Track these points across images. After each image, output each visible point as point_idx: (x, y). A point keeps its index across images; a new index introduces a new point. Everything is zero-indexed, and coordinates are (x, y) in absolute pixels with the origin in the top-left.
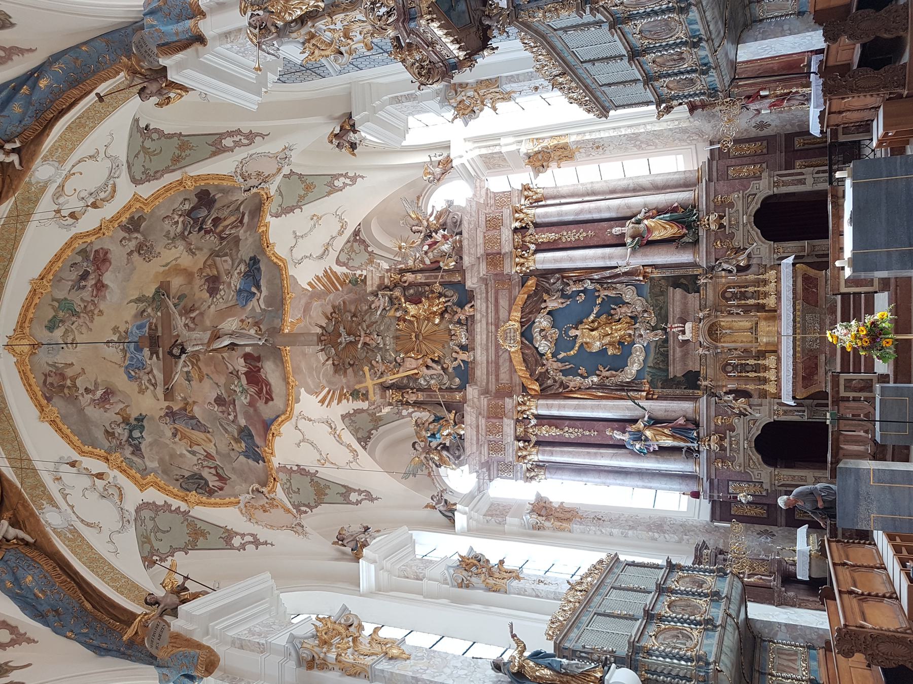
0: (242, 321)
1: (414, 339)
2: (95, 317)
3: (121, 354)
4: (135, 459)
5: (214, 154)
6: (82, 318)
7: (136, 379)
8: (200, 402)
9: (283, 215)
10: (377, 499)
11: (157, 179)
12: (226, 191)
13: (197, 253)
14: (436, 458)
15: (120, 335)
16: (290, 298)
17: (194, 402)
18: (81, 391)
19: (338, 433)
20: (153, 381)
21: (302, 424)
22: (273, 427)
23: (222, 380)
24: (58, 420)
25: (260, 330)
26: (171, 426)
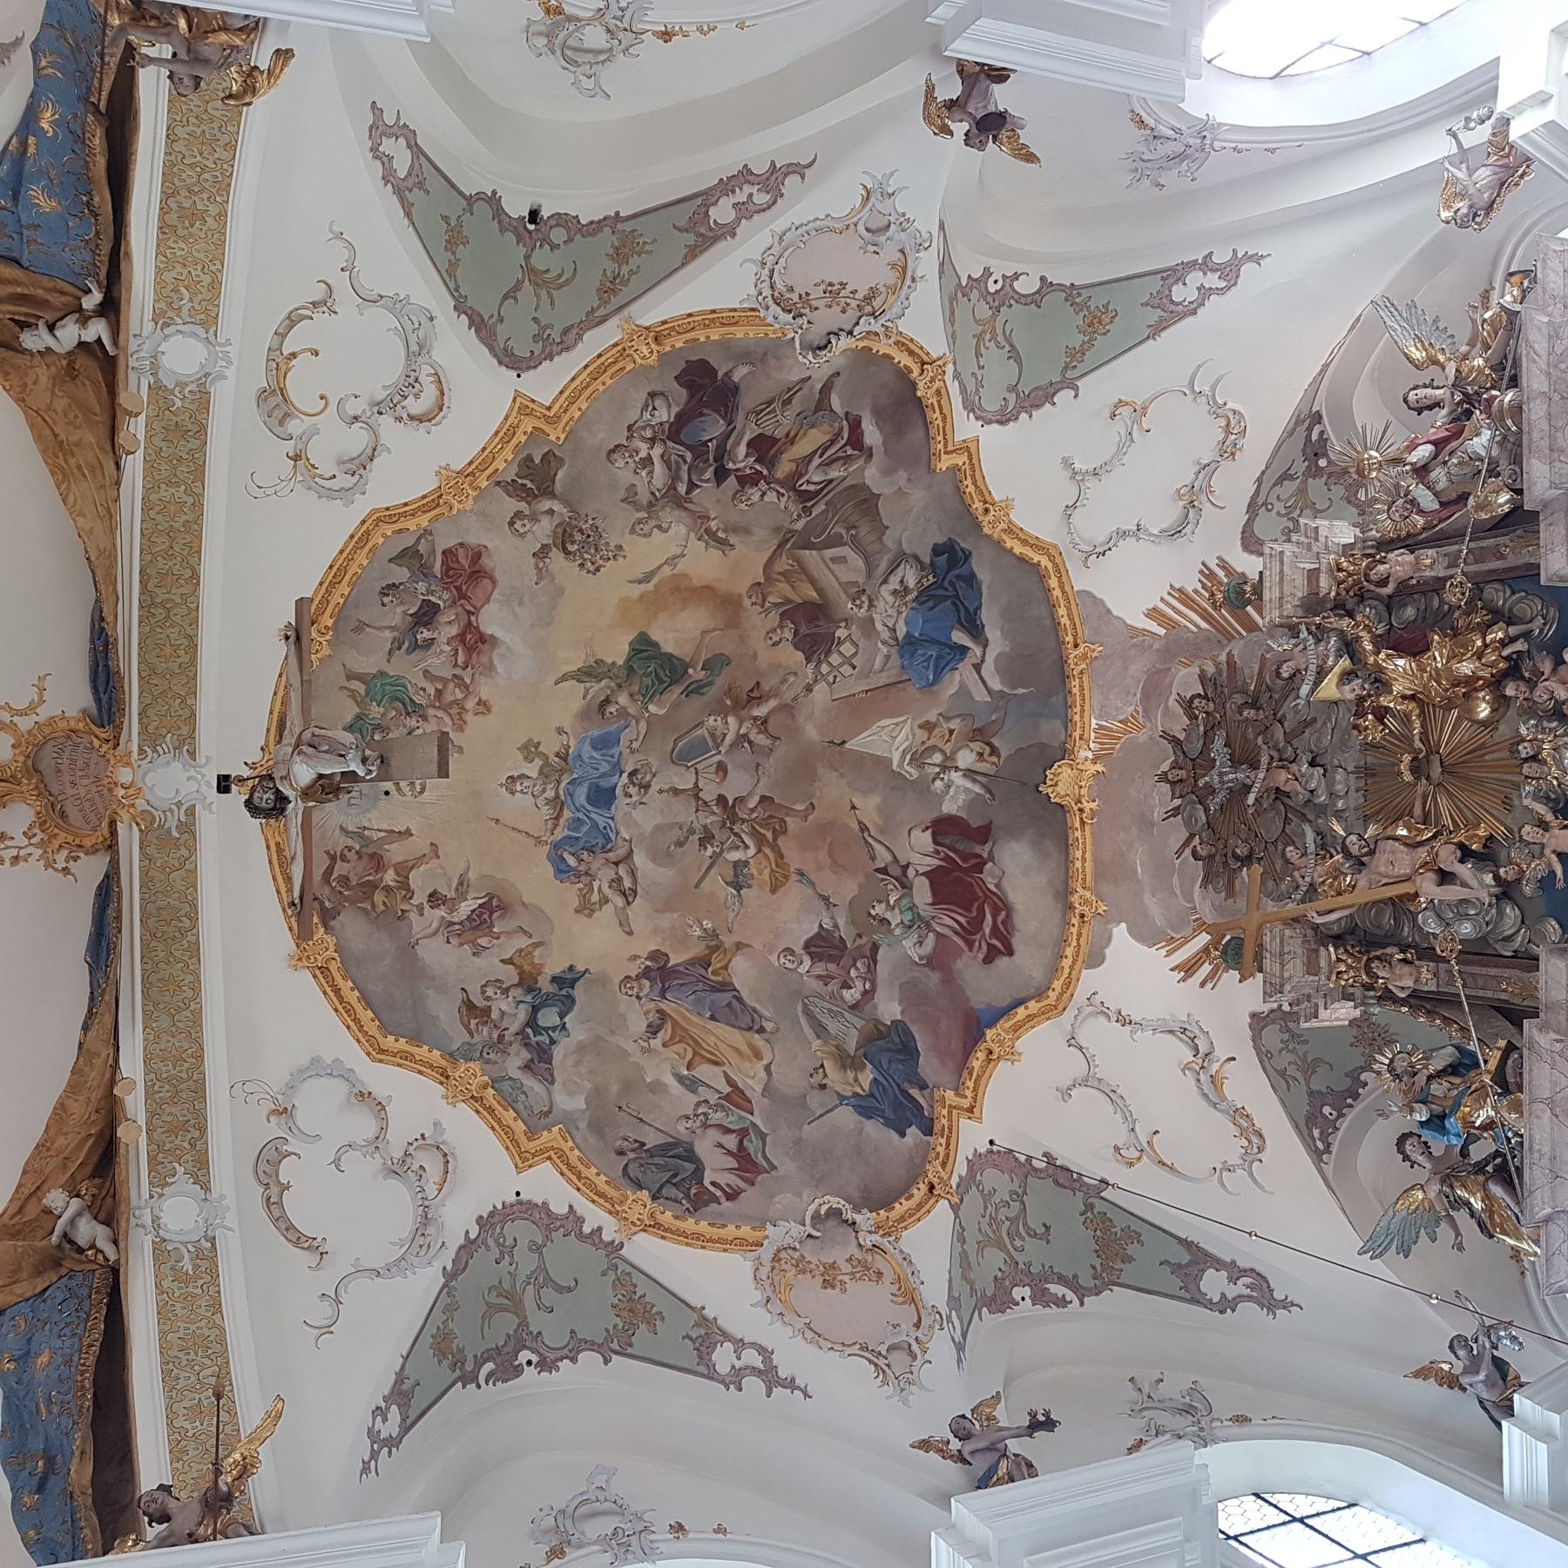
0: (928, 727)
1: (1408, 777)
2: (469, 717)
4: (529, 1082)
5: (693, 253)
6: (433, 721)
10: (1287, 1305)
11: (568, 349)
12: (763, 355)
14: (1477, 1204)
15: (546, 763)
16: (1084, 657)
17: (739, 946)
18: (420, 898)
19: (1215, 1067)
20: (627, 883)
21: (1096, 1033)
22: (990, 1034)
23: (846, 889)
24: (333, 967)
25: (994, 751)
26: (653, 1005)
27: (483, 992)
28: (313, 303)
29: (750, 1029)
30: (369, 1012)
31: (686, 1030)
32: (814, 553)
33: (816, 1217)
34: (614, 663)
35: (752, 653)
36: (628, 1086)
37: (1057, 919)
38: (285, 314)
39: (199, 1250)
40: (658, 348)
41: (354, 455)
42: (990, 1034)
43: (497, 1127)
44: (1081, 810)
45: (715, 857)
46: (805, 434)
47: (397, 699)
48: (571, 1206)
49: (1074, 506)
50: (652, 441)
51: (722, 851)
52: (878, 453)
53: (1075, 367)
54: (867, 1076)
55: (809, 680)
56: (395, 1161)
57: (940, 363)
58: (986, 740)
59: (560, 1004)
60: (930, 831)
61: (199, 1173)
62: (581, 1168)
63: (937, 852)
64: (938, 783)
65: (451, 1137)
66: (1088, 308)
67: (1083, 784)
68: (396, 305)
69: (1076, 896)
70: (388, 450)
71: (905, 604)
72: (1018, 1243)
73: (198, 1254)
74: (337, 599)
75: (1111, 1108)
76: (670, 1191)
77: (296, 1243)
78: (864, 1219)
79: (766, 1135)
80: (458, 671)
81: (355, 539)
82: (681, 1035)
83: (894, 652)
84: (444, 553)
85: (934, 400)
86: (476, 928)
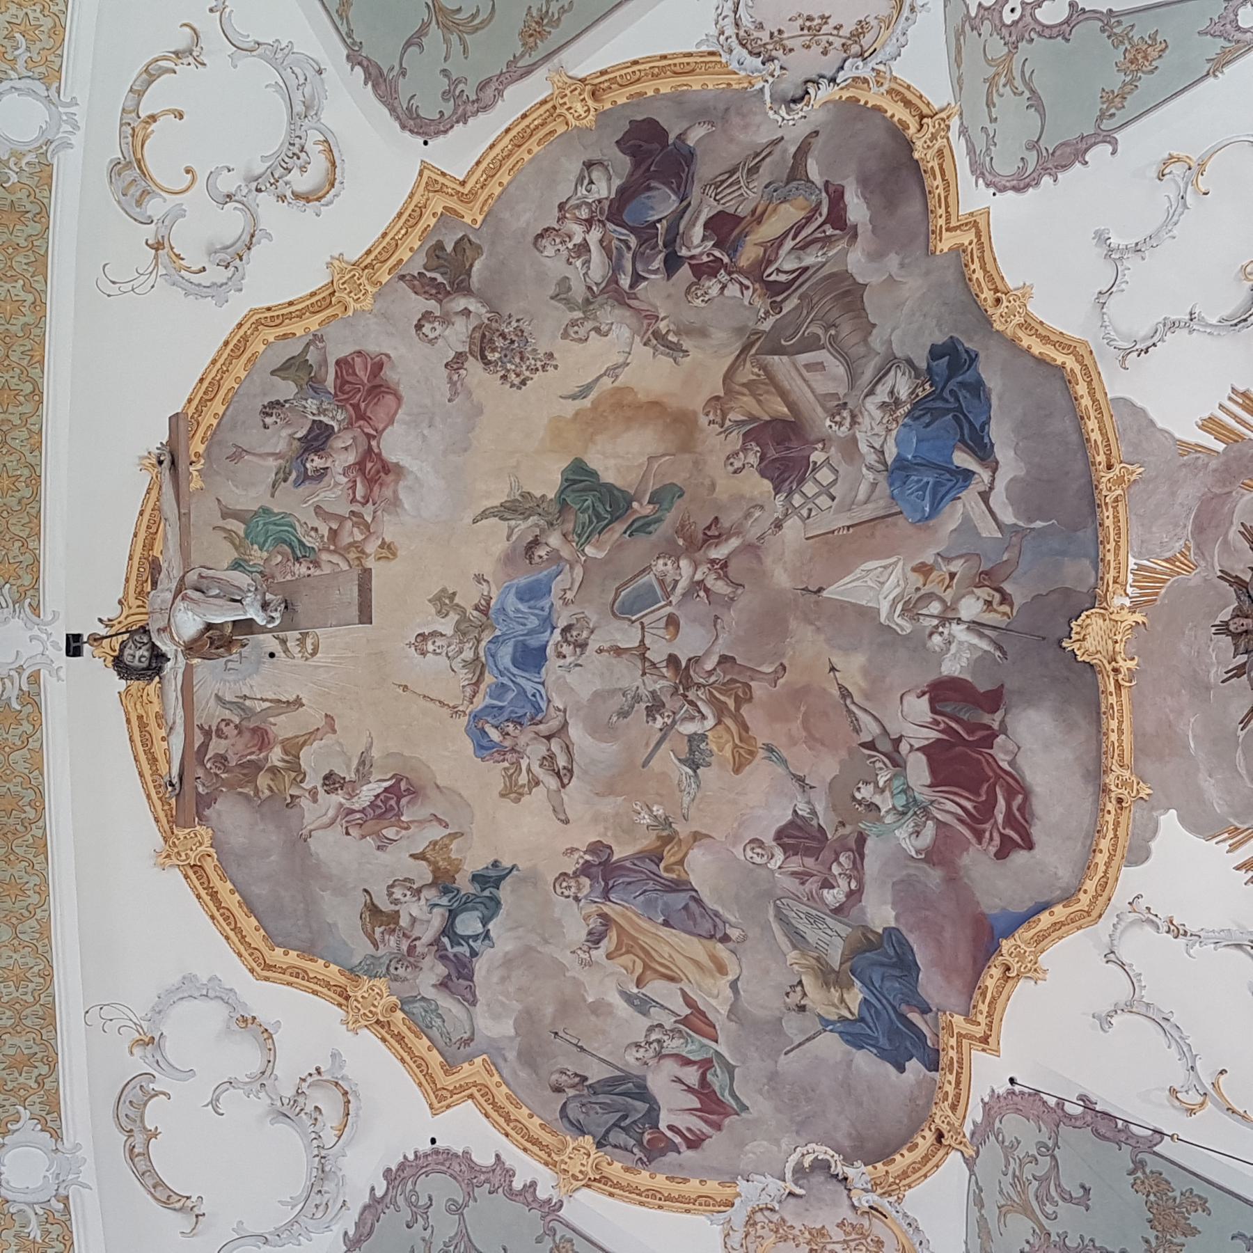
0: (924, 570)
3: (464, 676)
4: (446, 1003)
7: (503, 752)
8: (719, 836)
9: (1047, 180)
11: (485, 108)
13: (686, 344)
15: (464, 617)
16: (1120, 480)
17: (697, 837)
18: (313, 780)
20: (562, 762)
23: (826, 768)
24: (209, 865)
25: (1005, 599)
26: (593, 908)
27: (390, 894)
28: (176, 53)
29: (712, 937)
30: (253, 918)
31: (634, 939)
32: (785, 358)
33: (799, 1171)
34: (544, 496)
35: (707, 482)
36: (567, 1007)
37: (1088, 805)
38: (141, 67)
39: (49, 1212)
40: (596, 105)
41: (228, 243)
42: (1006, 945)
43: (407, 1058)
44: (1116, 670)
45: (666, 730)
46: (775, 210)
47: (284, 542)
48: (497, 1156)
49: (1109, 292)
50: (589, 222)
51: (674, 722)
52: (864, 231)
53: (1113, 115)
54: (856, 996)
55: (779, 514)
56: (286, 1101)
57: (943, 115)
58: (995, 585)
59: (481, 907)
60: (926, 697)
61: (49, 1118)
62: (510, 1108)
63: (937, 723)
64: (937, 639)
65: (352, 1071)
66: (1130, 39)
67: (1118, 638)
68: (277, 55)
69: (1112, 776)
70: (269, 237)
71: (896, 420)
72: (1049, 1209)
73: (48, 1219)
74: (209, 420)
75: (1163, 1040)
76: (618, 1137)
77: (166, 1203)
78: (858, 1173)
79: (734, 1067)
80: (356, 508)
81: (231, 346)
82: (627, 945)
83: (882, 478)
84: (338, 363)
85: (935, 164)
86: (380, 817)
